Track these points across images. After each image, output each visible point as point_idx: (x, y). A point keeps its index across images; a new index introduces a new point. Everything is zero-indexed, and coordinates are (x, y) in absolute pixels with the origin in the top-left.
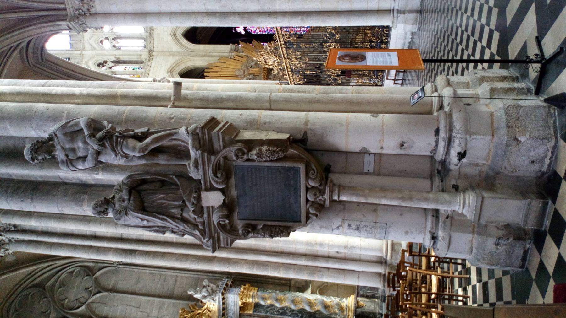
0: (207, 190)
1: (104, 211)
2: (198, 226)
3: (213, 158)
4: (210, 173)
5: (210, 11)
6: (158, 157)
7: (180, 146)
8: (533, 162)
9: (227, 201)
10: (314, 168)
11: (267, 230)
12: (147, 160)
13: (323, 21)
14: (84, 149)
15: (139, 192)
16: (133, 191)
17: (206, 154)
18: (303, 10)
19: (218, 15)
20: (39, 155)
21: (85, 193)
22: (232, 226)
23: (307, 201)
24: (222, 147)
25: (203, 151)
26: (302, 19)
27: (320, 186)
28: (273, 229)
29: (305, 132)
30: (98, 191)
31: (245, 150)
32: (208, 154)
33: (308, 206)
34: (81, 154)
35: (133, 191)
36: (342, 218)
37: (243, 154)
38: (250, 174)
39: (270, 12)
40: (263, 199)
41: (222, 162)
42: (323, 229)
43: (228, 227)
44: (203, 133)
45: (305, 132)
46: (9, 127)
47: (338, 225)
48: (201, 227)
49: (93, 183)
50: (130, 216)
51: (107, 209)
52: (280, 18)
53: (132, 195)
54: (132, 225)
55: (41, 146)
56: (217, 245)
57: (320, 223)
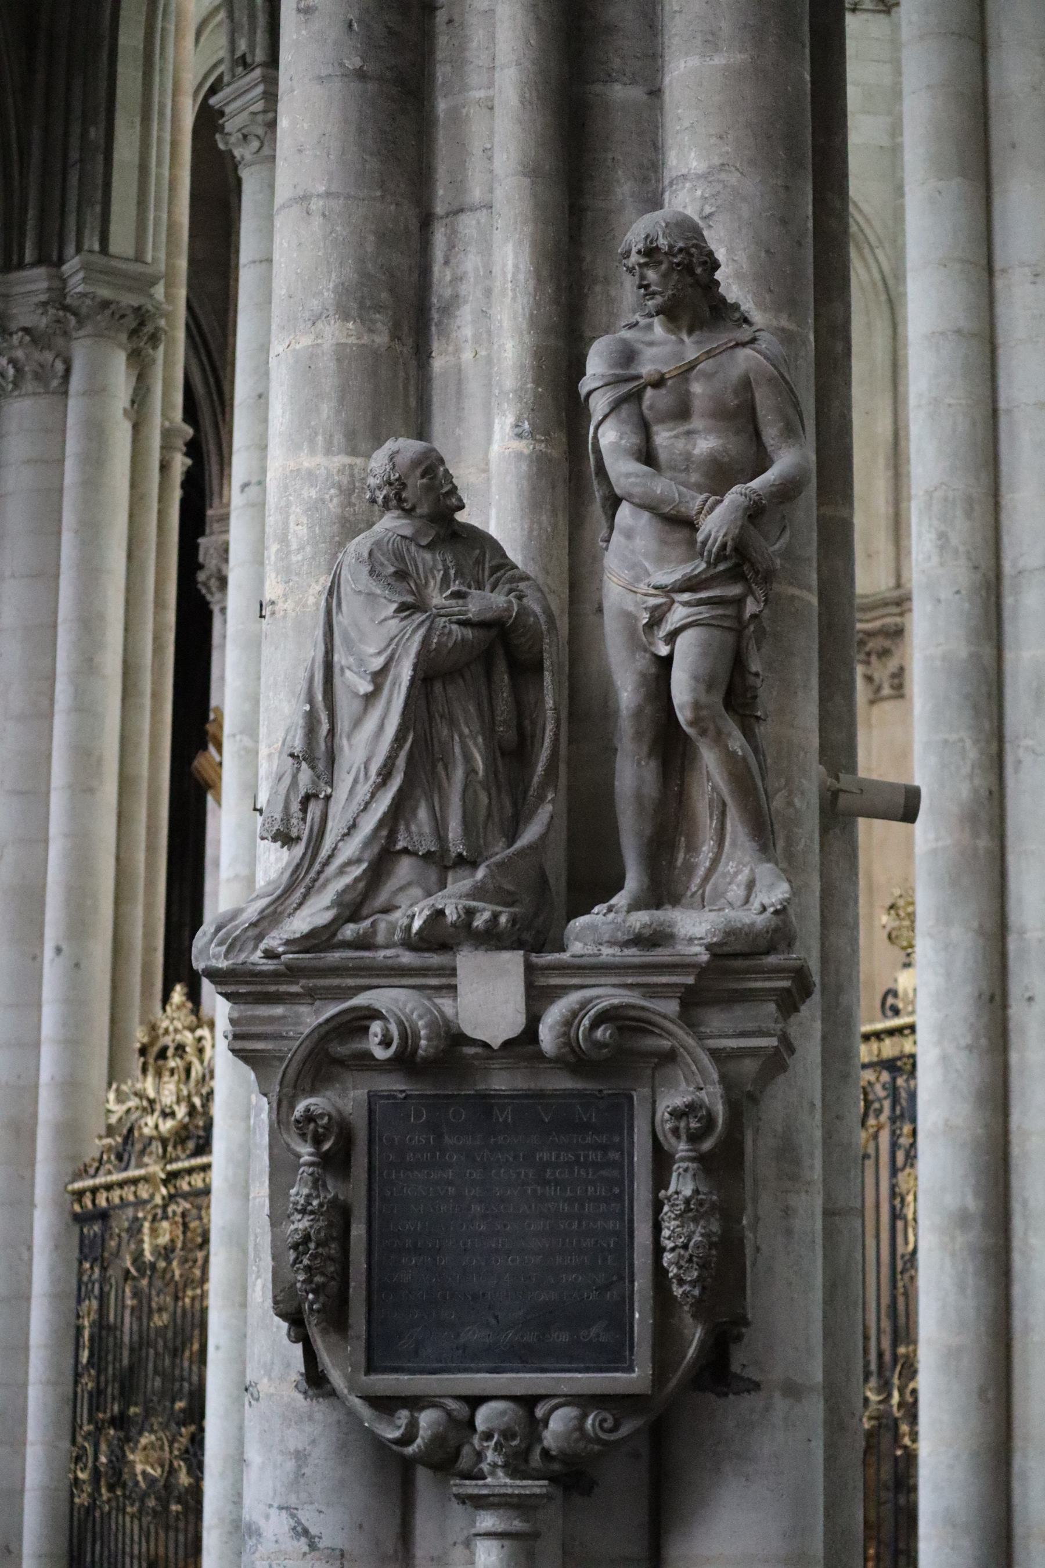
0: (530, 969)
1: (400, 500)
2: (354, 917)
3: (671, 1007)
4: (608, 995)
5: (1008, 601)
6: (650, 755)
7: (692, 848)
10: (624, 1430)
11: (330, 1225)
12: (638, 713)
13: (952, 1354)
14: (688, 457)
15: (487, 658)
16: (494, 632)
17: (690, 980)
18: (1018, 1223)
19: (988, 651)
20: (665, 276)
21: (395, 335)
22: (341, 1062)
23: (475, 1402)
24: (713, 1043)
25: (702, 971)
26: (963, 1219)
27: (546, 1453)
28: (333, 1249)
29: (755, 1386)
30: (406, 395)
31: (707, 1145)
32: (687, 986)
33: (452, 1405)
34: (663, 437)
35: (494, 632)
36: (347, 1547)
37: (694, 1138)
38: (592, 1156)
39: (1005, 1006)
40: (477, 1209)
41: (651, 1043)
42: (290, 1465)
43: (341, 1050)
44: (777, 971)
45: (756, 1386)
46: (719, 60)
47: (313, 1531)
48: (349, 931)
49: (439, 364)
50: (394, 625)
51: (409, 512)
52: (967, 1068)
53: (481, 633)
54: (341, 621)
55: (697, 283)
56: (243, 989)
57: (320, 1454)
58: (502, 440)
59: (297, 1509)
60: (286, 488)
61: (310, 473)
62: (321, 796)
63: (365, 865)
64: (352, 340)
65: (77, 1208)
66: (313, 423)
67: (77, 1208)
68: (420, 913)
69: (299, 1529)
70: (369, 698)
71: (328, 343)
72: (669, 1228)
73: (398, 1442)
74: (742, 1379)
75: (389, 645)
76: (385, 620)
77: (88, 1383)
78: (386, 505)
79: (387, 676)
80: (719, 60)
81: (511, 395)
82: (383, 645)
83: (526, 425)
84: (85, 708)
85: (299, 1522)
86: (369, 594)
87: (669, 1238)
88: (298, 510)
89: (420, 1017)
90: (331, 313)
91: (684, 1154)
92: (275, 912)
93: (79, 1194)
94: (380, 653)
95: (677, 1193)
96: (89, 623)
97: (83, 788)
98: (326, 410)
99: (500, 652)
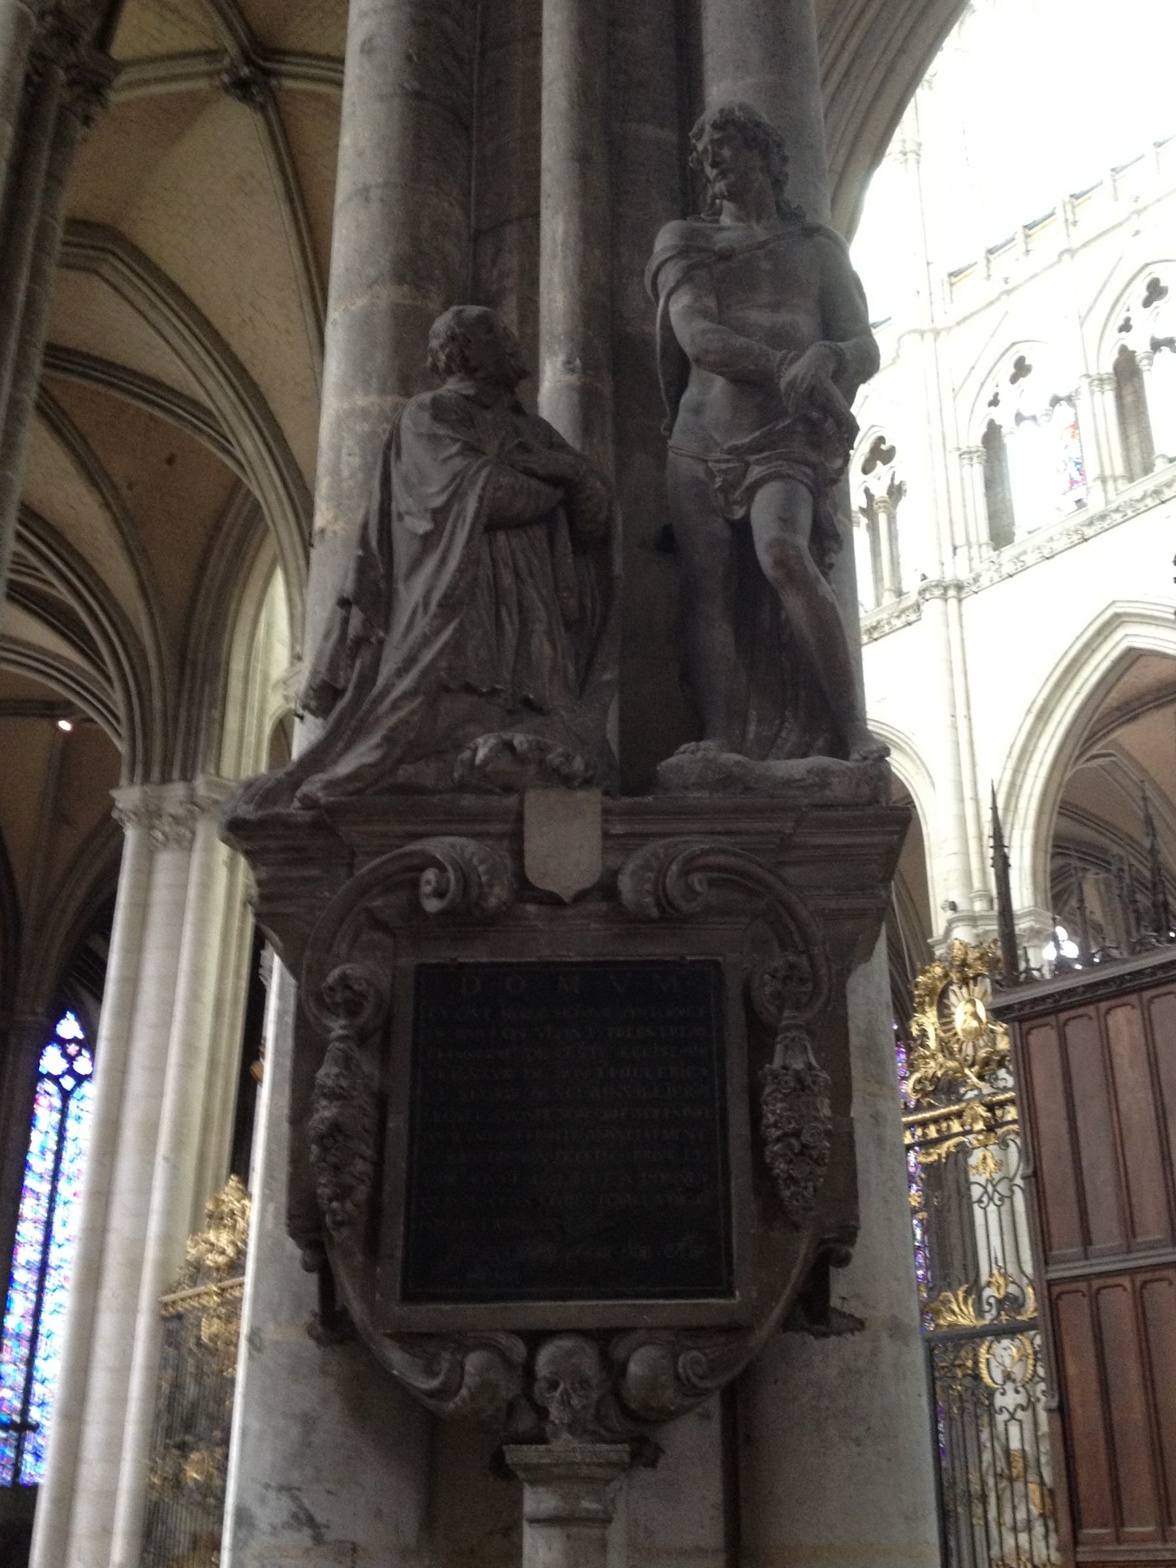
8: (170, 460)
9: (489, 768)
15: (546, 519)
16: (559, 494)
29: (859, 1325)
35: (559, 494)
42: (295, 1431)
46: (749, 80)
47: (320, 1518)
50: (458, 463)
58: (554, 374)
59: (299, 1490)
61: (363, 410)
63: (420, 699)
64: (408, 302)
65: (164, 1312)
67: (164, 1312)
69: (302, 1515)
70: (428, 541)
71: (383, 304)
72: (773, 1113)
73: (432, 1394)
74: (843, 1315)
76: (450, 457)
77: (164, 1422)
78: (449, 371)
79: (449, 512)
80: (749, 80)
82: (445, 481)
83: (578, 362)
84: (191, 1021)
85: (301, 1507)
87: (775, 1125)
89: (482, 862)
91: (788, 1022)
93: (166, 1305)
94: (443, 490)
95: (785, 1067)
96: (197, 973)
97: (187, 1066)
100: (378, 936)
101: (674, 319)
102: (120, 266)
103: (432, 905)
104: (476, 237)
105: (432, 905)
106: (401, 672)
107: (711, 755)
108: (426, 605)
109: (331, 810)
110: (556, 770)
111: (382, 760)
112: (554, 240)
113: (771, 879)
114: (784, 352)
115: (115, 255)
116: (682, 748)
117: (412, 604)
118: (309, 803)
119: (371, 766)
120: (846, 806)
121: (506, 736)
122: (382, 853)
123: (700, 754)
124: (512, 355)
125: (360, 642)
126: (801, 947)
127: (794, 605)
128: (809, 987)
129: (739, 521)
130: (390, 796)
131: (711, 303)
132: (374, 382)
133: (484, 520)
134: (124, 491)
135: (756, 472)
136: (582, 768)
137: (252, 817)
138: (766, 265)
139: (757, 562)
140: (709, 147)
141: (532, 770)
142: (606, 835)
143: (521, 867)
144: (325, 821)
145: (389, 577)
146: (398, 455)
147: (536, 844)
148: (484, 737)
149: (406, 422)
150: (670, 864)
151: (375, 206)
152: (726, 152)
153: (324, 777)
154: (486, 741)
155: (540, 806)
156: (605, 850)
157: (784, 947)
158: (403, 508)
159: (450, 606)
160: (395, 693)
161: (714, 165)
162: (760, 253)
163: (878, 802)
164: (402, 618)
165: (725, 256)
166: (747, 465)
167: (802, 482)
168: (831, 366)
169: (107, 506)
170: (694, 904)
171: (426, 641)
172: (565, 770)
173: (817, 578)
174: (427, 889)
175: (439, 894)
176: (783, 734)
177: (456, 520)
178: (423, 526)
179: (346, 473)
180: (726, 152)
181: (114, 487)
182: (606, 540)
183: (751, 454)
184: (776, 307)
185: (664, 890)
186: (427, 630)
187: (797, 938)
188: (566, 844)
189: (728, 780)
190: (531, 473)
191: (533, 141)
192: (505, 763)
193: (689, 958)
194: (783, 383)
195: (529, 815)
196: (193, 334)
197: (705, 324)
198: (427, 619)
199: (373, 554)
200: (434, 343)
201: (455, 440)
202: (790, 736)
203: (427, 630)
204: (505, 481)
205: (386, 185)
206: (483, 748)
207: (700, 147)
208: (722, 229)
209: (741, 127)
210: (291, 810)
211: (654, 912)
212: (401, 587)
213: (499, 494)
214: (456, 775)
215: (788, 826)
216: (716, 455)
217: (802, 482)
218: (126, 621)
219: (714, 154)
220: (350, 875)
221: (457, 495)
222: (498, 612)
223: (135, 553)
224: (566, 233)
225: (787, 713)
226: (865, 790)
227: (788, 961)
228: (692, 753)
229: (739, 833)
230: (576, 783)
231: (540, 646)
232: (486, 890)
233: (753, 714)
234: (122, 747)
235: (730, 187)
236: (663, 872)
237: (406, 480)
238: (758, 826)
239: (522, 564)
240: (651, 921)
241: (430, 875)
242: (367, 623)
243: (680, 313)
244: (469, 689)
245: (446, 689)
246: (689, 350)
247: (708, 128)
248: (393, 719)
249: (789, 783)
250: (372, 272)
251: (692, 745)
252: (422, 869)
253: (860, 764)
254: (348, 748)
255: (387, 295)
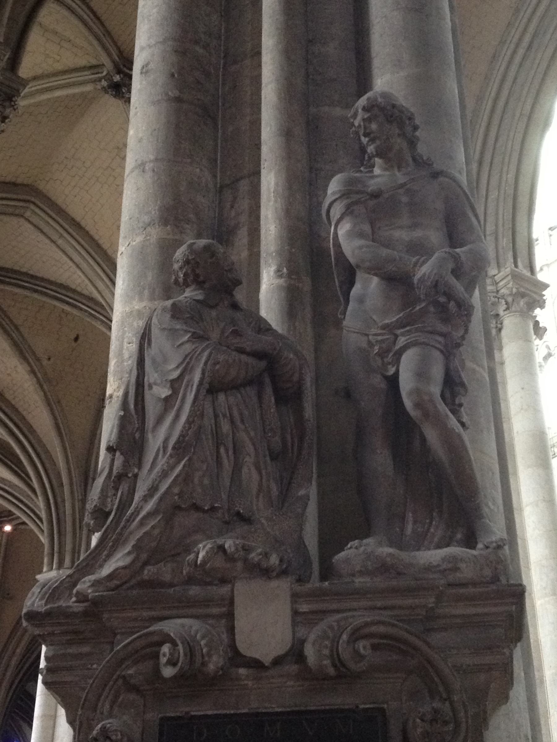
8: (76, 339)
15: (255, 381)
16: (263, 364)
35: (263, 364)
46: (402, 74)
54: (150, 354)
60: (123, 323)
61: (139, 311)
62: (130, 475)
64: (170, 237)
66: (142, 283)
68: (203, 549)
70: (168, 402)
71: (154, 239)
75: (184, 360)
76: (182, 344)
78: (186, 284)
80: (402, 74)
81: (274, 254)
82: (180, 360)
83: (285, 270)
86: (170, 330)
88: (130, 335)
89: (203, 637)
90: (156, 221)
92: (87, 565)
94: (177, 367)
98: (150, 276)
99: (267, 380)
100: (132, 696)
101: (341, 239)
102: (37, 210)
103: (168, 672)
104: (221, 190)
105: (168, 672)
106: (146, 498)
107: (369, 550)
108: (165, 448)
109: (95, 602)
110: (257, 566)
111: (133, 562)
112: (269, 189)
113: (418, 643)
114: (418, 257)
115: (34, 203)
116: (349, 546)
117: (157, 447)
118: (82, 598)
119: (125, 568)
120: (474, 584)
121: (220, 541)
122: (133, 633)
123: (362, 549)
124: (230, 270)
125: (120, 477)
126: (444, 696)
127: (431, 435)
128: (451, 727)
129: (392, 376)
130: (139, 590)
131: (367, 228)
132: (146, 292)
133: (207, 386)
134: (45, 362)
135: (402, 341)
136: (277, 562)
137: (43, 610)
138: (405, 199)
139: (403, 404)
140: (362, 124)
141: (240, 565)
142: (295, 613)
143: (233, 640)
144: (94, 609)
145: (142, 429)
146: (149, 344)
147: (243, 622)
148: (204, 543)
149: (155, 320)
150: (342, 633)
151: (149, 175)
152: (374, 126)
153: (92, 578)
154: (204, 547)
155: (245, 592)
156: (294, 624)
157: (432, 697)
158: (152, 381)
159: (181, 448)
160: (143, 513)
161: (365, 135)
162: (401, 191)
163: (499, 580)
164: (149, 457)
165: (376, 195)
166: (396, 336)
167: (436, 348)
168: (451, 265)
169: (33, 372)
170: (362, 664)
171: (164, 474)
172: (264, 565)
173: (447, 415)
174: (163, 660)
175: (172, 663)
176: (432, 530)
177: (187, 386)
178: (165, 392)
179: (126, 355)
180: (374, 126)
181: (38, 360)
182: (298, 395)
183: (399, 329)
184: (414, 226)
185: (338, 655)
186: (165, 467)
187: (441, 689)
188: (265, 622)
189: (384, 568)
190: (241, 351)
191: (256, 124)
192: (219, 562)
193: (362, 706)
194: (416, 280)
195: (237, 600)
196: (88, 252)
197: (362, 242)
198: (165, 459)
199: (131, 414)
200: (176, 266)
201: (186, 331)
202: (438, 531)
203: (165, 467)
204: (221, 358)
205: (156, 160)
206: (203, 550)
207: (356, 124)
208: (373, 177)
209: (382, 109)
210: (70, 604)
211: (332, 671)
212: (150, 436)
213: (218, 367)
214: (184, 572)
215: (431, 601)
216: (374, 331)
217: (436, 348)
218: (47, 452)
219: (365, 128)
220: (112, 650)
221: (186, 369)
222: (218, 452)
223: (52, 404)
224: (277, 184)
225: (434, 514)
226: (487, 572)
227: (433, 708)
228: (356, 548)
229: (393, 608)
230: (274, 574)
231: (250, 475)
232: (206, 659)
233: (410, 516)
234: (44, 539)
235: (377, 148)
236: (336, 641)
237: (154, 361)
238: (409, 601)
239: (236, 413)
240: (327, 677)
241: (166, 649)
242: (126, 464)
243: (345, 236)
244: (196, 508)
245: (178, 508)
246: (352, 260)
247: (360, 110)
248: (139, 534)
249: (429, 568)
250: (146, 219)
251: (356, 542)
252: (160, 644)
253: (484, 553)
254: (109, 556)
255: (155, 233)
